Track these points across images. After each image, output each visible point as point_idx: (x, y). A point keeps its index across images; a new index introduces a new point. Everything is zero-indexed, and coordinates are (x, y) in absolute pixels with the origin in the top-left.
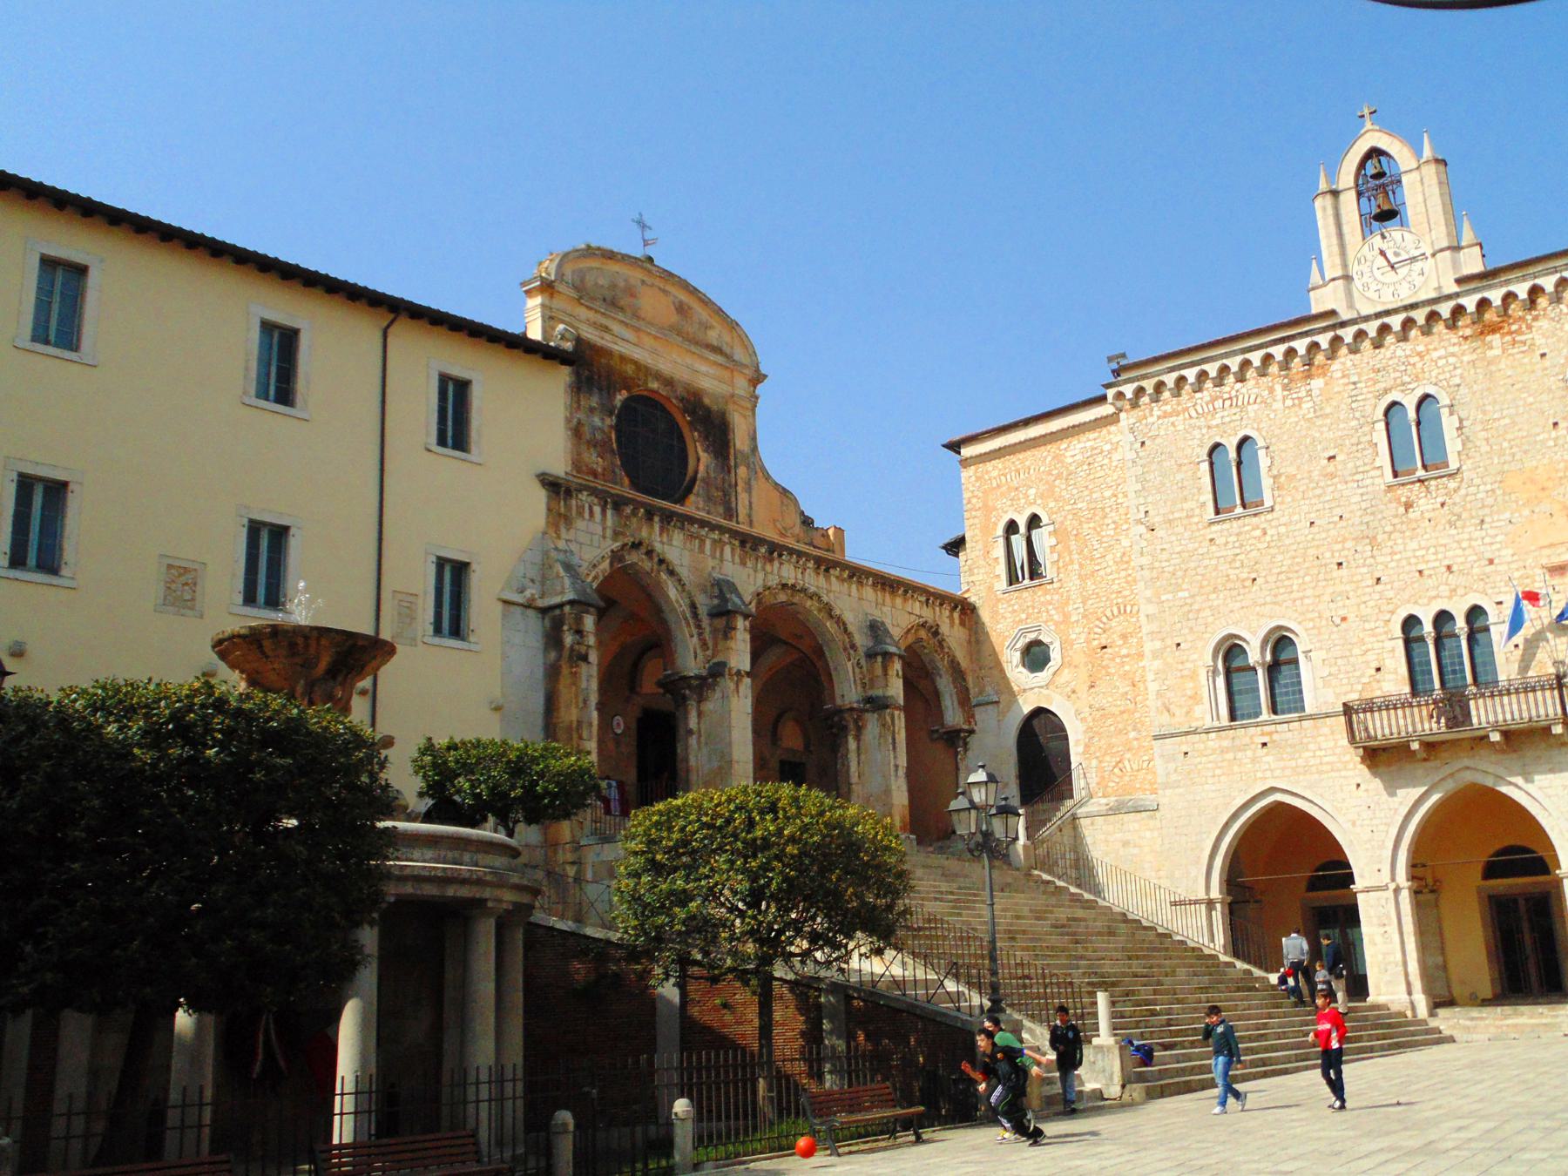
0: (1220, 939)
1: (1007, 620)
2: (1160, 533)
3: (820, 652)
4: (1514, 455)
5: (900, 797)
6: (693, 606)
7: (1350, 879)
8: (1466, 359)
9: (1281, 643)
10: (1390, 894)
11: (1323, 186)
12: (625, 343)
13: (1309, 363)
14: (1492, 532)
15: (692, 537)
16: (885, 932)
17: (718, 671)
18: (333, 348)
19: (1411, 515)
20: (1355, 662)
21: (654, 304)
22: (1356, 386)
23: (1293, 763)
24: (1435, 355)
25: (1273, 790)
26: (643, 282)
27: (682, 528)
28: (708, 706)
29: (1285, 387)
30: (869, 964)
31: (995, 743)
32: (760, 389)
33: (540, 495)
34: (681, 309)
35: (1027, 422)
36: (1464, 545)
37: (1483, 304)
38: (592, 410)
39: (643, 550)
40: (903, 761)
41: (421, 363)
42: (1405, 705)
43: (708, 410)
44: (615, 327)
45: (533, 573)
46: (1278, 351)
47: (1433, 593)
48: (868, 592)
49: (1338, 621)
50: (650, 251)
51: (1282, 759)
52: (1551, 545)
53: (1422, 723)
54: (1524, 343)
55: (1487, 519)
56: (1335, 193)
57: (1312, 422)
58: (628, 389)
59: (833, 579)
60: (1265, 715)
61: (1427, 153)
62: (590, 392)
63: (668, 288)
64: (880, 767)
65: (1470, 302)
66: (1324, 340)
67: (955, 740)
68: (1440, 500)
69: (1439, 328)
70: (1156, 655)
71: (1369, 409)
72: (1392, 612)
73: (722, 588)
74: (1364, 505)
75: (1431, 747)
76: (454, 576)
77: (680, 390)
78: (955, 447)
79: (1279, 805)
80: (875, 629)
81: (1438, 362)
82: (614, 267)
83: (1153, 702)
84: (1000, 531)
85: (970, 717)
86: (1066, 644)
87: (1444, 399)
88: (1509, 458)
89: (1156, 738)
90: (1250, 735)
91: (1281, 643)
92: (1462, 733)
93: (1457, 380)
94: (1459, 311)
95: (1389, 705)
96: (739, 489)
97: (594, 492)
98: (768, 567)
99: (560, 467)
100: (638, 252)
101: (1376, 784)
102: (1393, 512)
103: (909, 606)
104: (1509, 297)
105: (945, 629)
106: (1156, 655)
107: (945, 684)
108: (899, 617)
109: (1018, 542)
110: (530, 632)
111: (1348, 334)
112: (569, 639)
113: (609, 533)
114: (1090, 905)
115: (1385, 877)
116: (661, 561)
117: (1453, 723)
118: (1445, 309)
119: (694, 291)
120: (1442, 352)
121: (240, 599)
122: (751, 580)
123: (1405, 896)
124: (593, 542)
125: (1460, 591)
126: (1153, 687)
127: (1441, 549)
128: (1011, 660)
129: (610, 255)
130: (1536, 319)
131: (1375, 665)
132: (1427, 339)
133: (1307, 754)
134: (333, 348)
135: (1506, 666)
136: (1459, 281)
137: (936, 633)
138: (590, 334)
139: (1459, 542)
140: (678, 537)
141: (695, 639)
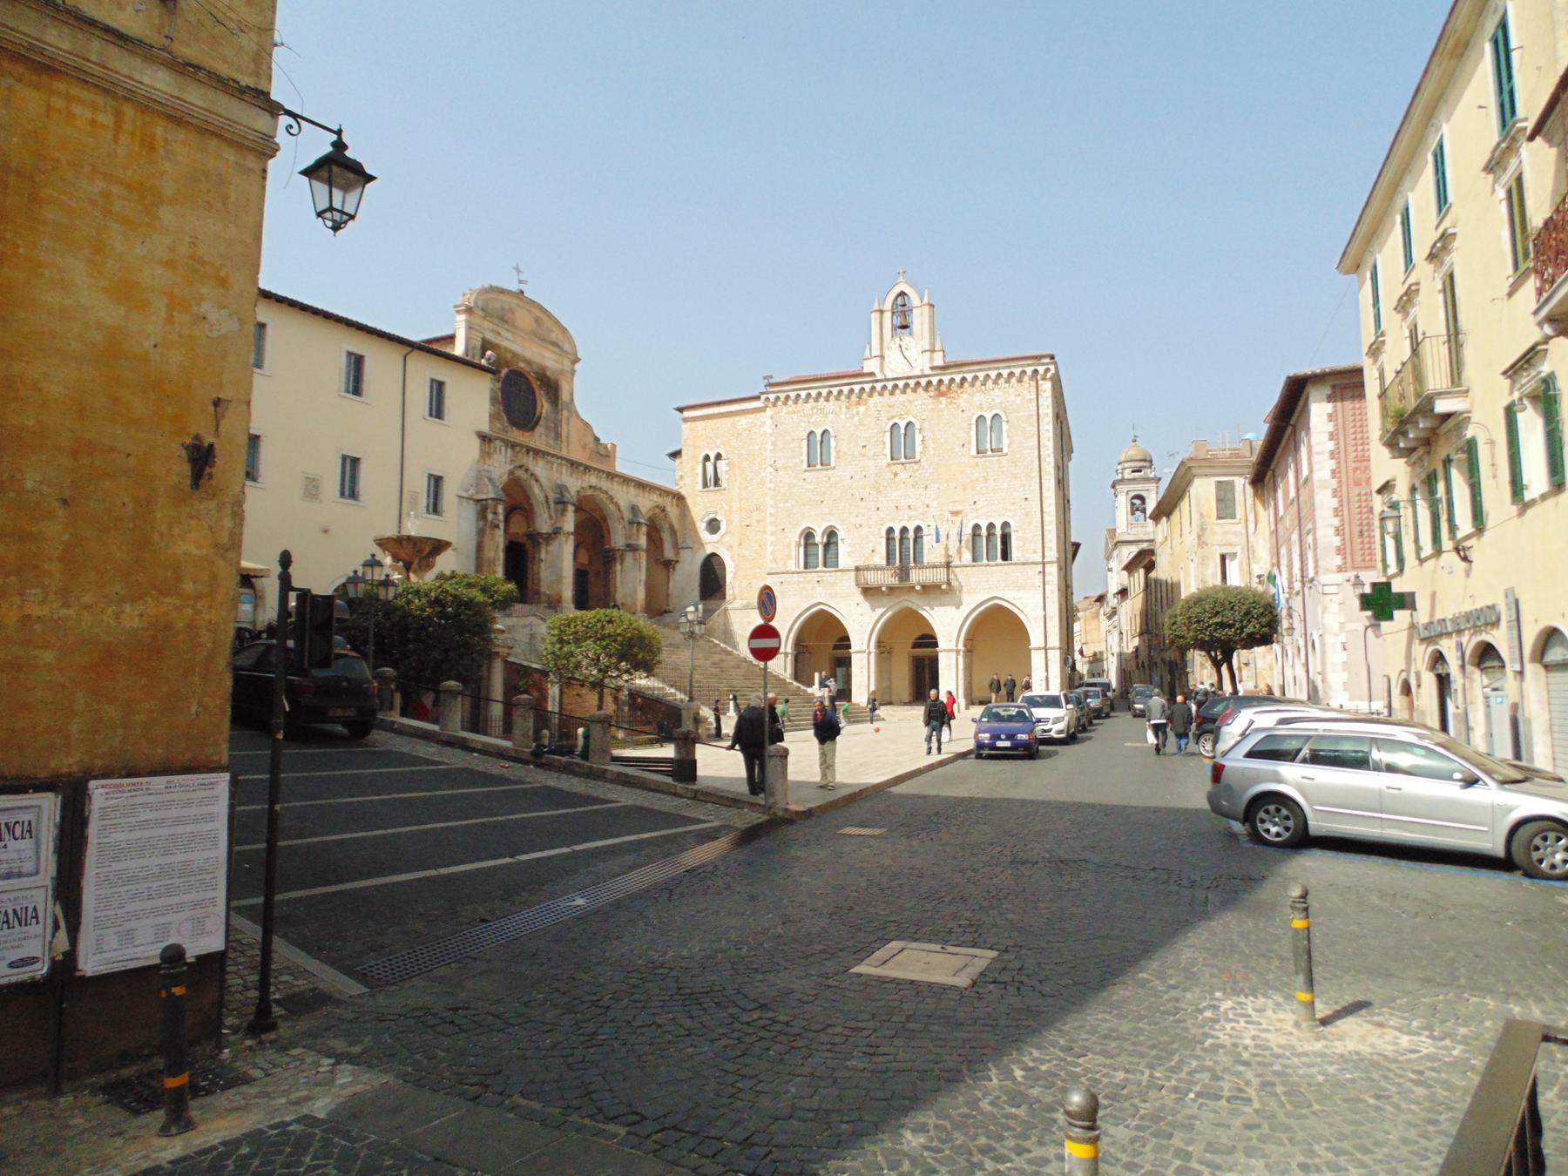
0: (789, 670)
1: (701, 506)
3: (605, 519)
5: (641, 595)
7: (849, 647)
9: (831, 534)
11: (876, 307)
12: (512, 343)
13: (860, 397)
16: (648, 668)
17: (557, 532)
18: (381, 366)
20: (862, 547)
21: (523, 319)
22: (880, 411)
28: (551, 548)
30: (642, 681)
31: (687, 575)
32: (577, 366)
33: (476, 442)
34: (538, 321)
35: (719, 404)
37: (941, 382)
40: (643, 577)
41: (423, 371)
42: (882, 569)
43: (549, 379)
44: (503, 332)
45: (473, 482)
46: (846, 389)
48: (632, 490)
50: (523, 287)
53: (888, 578)
56: (882, 312)
57: (857, 426)
60: (821, 568)
61: (926, 300)
64: (631, 580)
65: (935, 380)
66: (867, 387)
67: (669, 565)
69: (920, 390)
70: (773, 533)
73: (561, 489)
75: (891, 589)
76: (436, 482)
77: (535, 368)
78: (681, 410)
79: (822, 611)
80: (634, 509)
81: (916, 407)
82: (503, 297)
83: (769, 557)
84: (701, 459)
85: (677, 554)
86: (729, 522)
87: (918, 426)
91: (831, 534)
92: (906, 584)
94: (929, 383)
95: (876, 568)
97: (503, 440)
99: (485, 427)
100: (514, 287)
101: (866, 605)
104: (952, 380)
105: (668, 509)
106: (773, 533)
107: (666, 536)
108: (646, 503)
109: (710, 466)
110: (470, 511)
111: (879, 386)
112: (490, 517)
114: (730, 653)
115: (865, 647)
117: (901, 579)
118: (923, 382)
119: (545, 311)
121: (338, 494)
122: (574, 484)
123: (873, 656)
124: (501, 466)
126: (770, 549)
128: (701, 526)
129: (502, 291)
134: (381, 366)
135: (928, 558)
136: (933, 368)
140: (541, 463)
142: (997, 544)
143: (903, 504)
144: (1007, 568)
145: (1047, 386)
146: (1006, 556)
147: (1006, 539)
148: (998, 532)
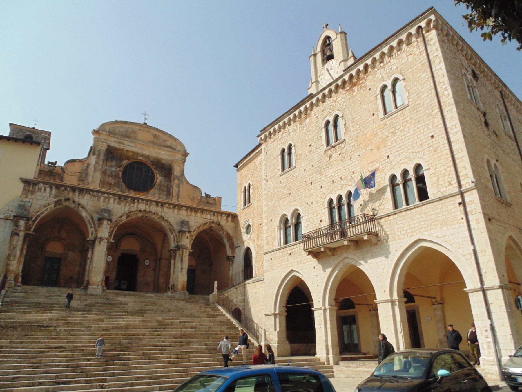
2: (269, 182)
4: (360, 130)
6: (92, 218)
8: (347, 98)
10: (322, 311)
14: (354, 161)
15: (94, 196)
19: (331, 160)
21: (142, 135)
23: (297, 260)
24: (339, 100)
25: (292, 271)
26: (140, 129)
27: (89, 194)
29: (300, 124)
36: (346, 168)
38: (112, 166)
39: (71, 201)
44: (126, 143)
47: (336, 189)
49: (310, 204)
51: (294, 259)
52: (371, 163)
54: (364, 87)
55: (353, 156)
56: (315, 55)
58: (129, 159)
59: (165, 208)
62: (112, 161)
63: (150, 131)
68: (339, 153)
71: (320, 125)
72: (325, 198)
74: (318, 160)
82: (126, 126)
88: (359, 131)
89: (265, 254)
90: (288, 250)
93: (344, 107)
96: (174, 187)
98: (132, 205)
102: (326, 160)
103: (204, 216)
113: (52, 196)
116: (79, 204)
119: (157, 129)
120: (341, 98)
125: (344, 186)
127: (339, 171)
129: (126, 123)
130: (367, 77)
131: (320, 220)
132: (336, 95)
133: (301, 256)
137: (219, 225)
138: (113, 144)
139: (344, 167)
140: (87, 197)
141: (93, 228)
142: (415, 186)
143: (336, 178)
144: (427, 208)
145: (432, 36)
146: (423, 195)
147: (421, 180)
148: (412, 175)
